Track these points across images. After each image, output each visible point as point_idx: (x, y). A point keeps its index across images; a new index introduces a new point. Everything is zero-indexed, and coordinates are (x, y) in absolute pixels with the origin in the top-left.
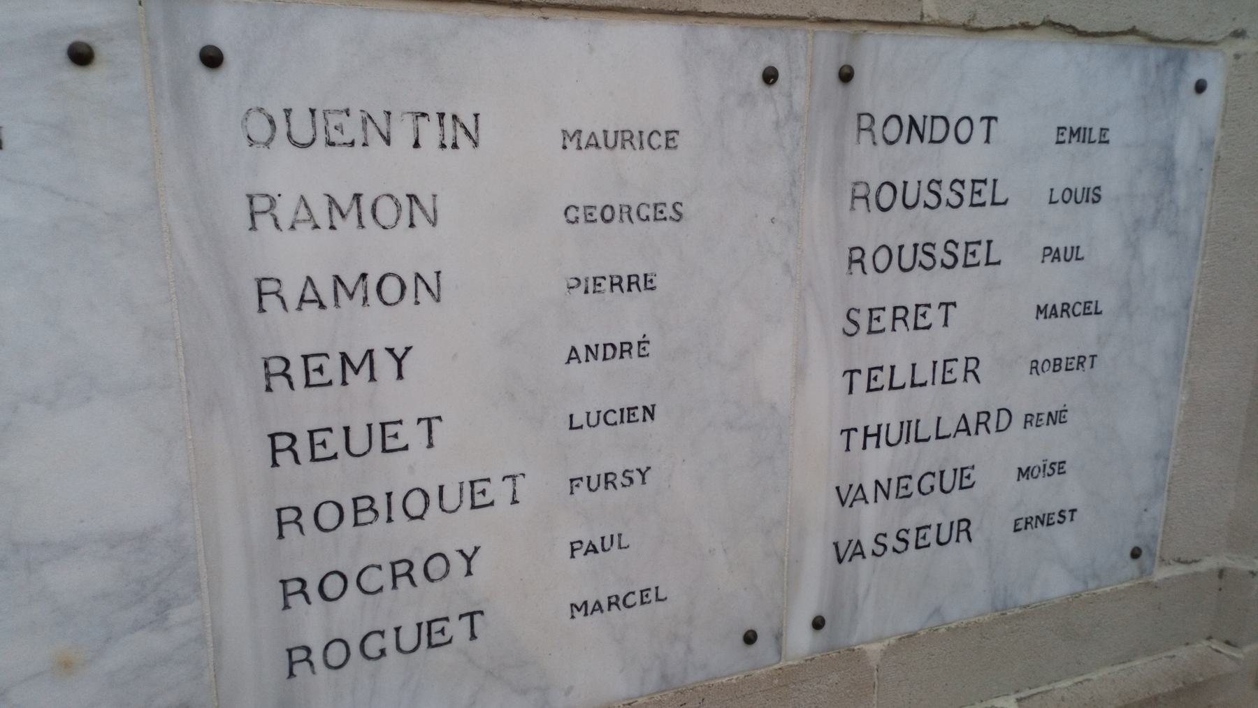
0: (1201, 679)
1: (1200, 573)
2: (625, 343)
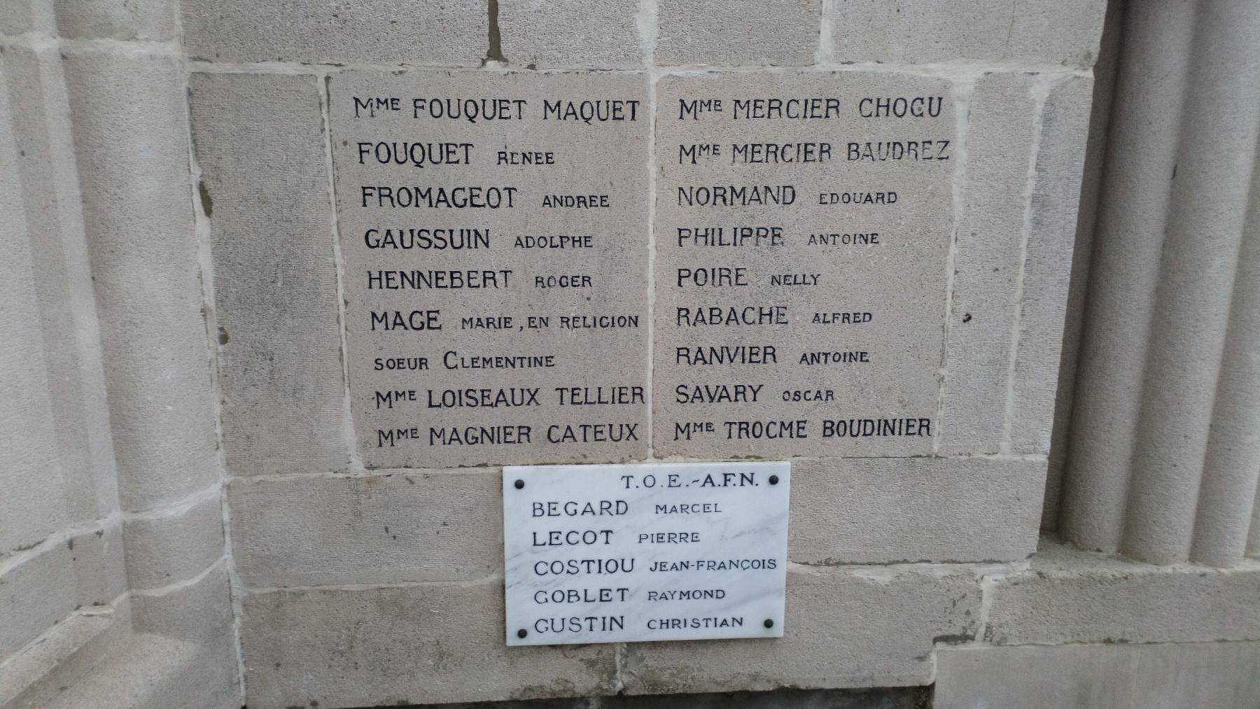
0: (75, 649)
1: (48, 552)
2: (925, 420)
